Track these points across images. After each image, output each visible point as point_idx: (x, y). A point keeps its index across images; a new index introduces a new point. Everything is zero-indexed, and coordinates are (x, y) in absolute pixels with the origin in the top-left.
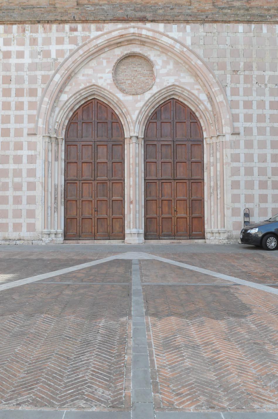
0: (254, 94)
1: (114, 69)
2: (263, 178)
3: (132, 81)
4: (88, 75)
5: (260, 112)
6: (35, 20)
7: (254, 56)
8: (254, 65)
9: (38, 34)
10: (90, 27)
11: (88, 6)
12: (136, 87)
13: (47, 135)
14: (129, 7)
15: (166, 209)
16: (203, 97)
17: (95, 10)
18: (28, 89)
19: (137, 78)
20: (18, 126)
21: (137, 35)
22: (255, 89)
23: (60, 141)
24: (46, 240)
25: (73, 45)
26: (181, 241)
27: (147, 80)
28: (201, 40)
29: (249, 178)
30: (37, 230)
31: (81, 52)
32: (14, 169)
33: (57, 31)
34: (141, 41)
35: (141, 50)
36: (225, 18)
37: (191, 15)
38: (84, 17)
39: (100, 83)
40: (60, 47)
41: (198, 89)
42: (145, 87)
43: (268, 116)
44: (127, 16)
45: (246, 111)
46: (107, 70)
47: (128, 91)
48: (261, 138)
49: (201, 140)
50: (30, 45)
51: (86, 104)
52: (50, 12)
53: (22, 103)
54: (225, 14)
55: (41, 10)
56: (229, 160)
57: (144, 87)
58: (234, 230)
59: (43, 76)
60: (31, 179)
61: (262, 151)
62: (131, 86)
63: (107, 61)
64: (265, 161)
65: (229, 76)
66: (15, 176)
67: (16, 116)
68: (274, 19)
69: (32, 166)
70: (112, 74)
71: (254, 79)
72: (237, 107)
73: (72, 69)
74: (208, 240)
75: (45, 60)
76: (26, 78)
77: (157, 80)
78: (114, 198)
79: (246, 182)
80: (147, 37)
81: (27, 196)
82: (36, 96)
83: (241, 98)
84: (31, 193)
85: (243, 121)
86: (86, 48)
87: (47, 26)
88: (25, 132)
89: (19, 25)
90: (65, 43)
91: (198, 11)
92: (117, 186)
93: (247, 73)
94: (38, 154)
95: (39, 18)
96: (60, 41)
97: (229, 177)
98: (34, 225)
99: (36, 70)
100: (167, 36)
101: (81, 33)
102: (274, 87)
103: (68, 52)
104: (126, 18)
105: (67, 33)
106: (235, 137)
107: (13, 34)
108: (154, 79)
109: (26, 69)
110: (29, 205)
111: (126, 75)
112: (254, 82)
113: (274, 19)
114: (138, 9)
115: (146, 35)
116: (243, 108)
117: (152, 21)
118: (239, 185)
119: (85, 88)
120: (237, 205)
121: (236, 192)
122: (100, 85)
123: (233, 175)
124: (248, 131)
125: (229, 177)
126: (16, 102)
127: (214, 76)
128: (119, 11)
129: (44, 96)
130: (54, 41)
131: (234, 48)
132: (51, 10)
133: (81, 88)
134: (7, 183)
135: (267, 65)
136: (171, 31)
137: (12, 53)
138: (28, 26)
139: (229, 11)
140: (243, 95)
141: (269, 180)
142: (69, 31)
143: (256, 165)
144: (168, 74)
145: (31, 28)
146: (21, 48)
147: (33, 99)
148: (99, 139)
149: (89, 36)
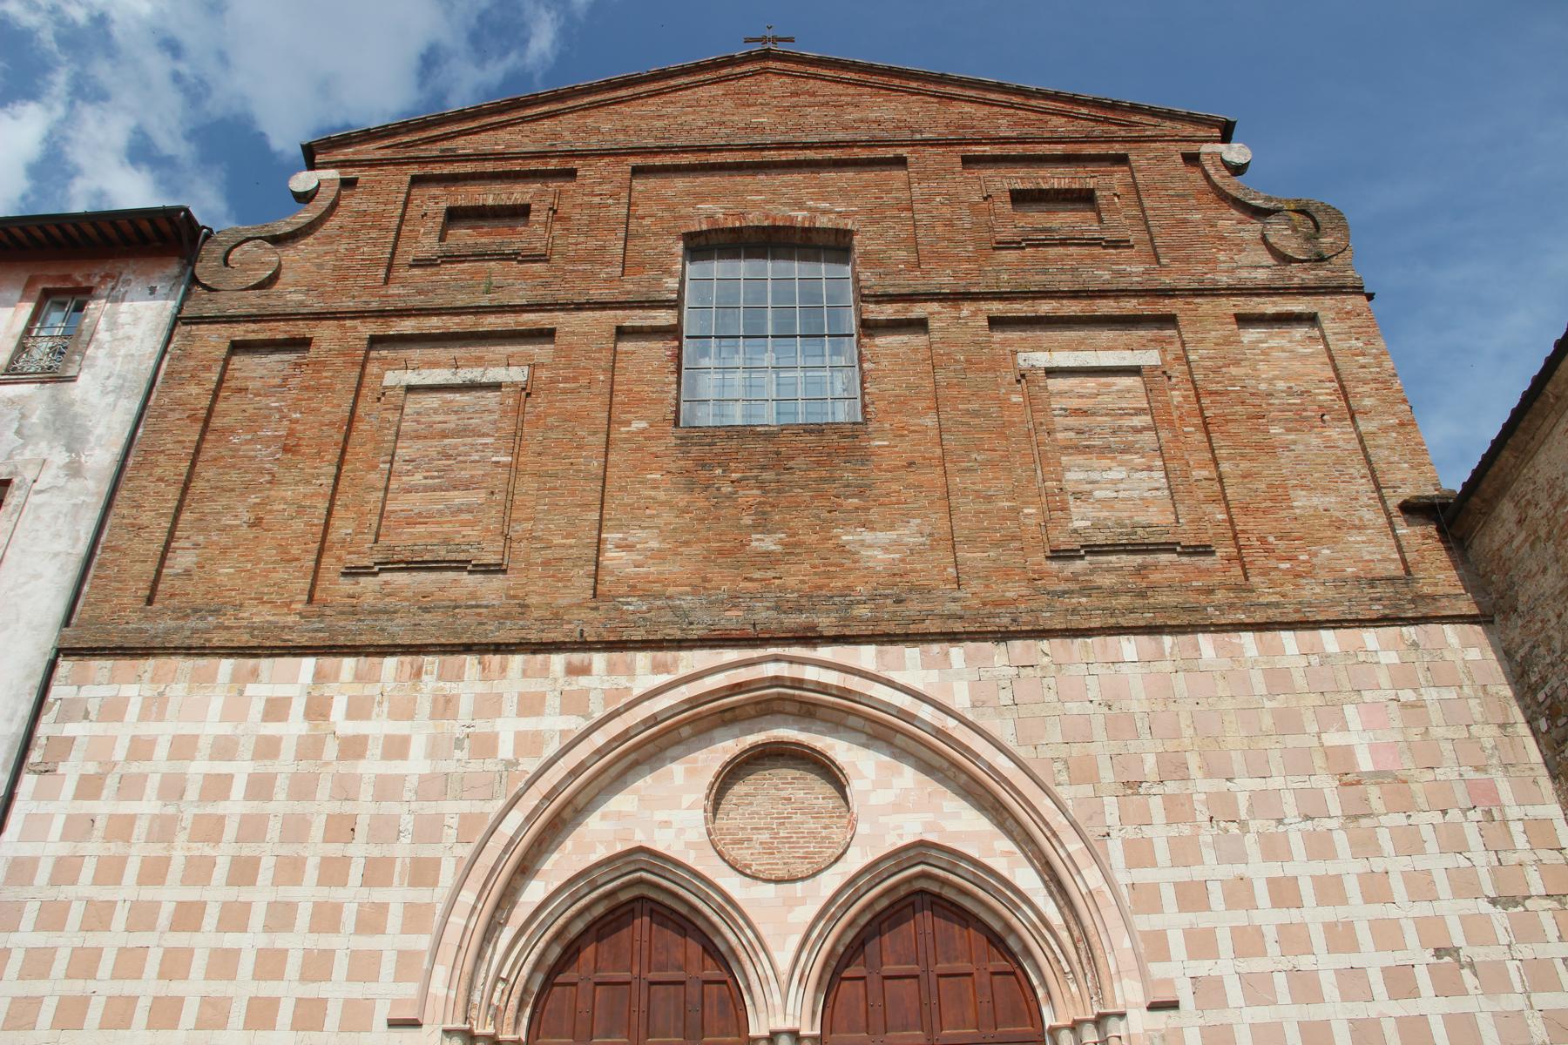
0: (1209, 856)
3: (775, 836)
4: (620, 815)
6: (457, 641)
8: (1193, 761)
9: (461, 684)
10: (633, 661)
11: (629, 599)
13: (459, 1025)
16: (1027, 879)
17: (649, 611)
18: (408, 861)
19: (790, 823)
20: (358, 990)
21: (788, 684)
22: (1210, 839)
27: (825, 828)
33: (525, 673)
36: (1076, 622)
38: (613, 630)
39: (662, 843)
40: (528, 724)
42: (821, 852)
43: (1271, 934)
45: (1188, 918)
46: (687, 799)
47: (761, 868)
55: (479, 614)
57: (815, 853)
59: (464, 818)
62: (769, 849)
65: (1111, 805)
68: (1232, 617)
70: (705, 811)
71: (1198, 806)
72: (1156, 907)
76: (407, 822)
77: (862, 828)
82: (435, 884)
83: (1164, 875)
86: (616, 727)
87: (494, 660)
89: (403, 658)
91: (984, 604)
93: (1171, 787)
95: (469, 634)
96: (530, 705)
99: (443, 795)
101: (603, 681)
102: (1274, 830)
104: (751, 630)
105: (556, 680)
107: (380, 685)
108: (852, 825)
109: (407, 795)
113: (1232, 617)
114: (790, 604)
115: (819, 683)
122: (660, 847)
126: (360, 905)
130: (510, 705)
131: (1115, 710)
132: (508, 613)
135: (1237, 757)
136: (901, 667)
137: (370, 742)
139: (1084, 600)
142: (563, 674)
144: (897, 807)
145: (442, 666)
146: (400, 728)
147: (421, 895)
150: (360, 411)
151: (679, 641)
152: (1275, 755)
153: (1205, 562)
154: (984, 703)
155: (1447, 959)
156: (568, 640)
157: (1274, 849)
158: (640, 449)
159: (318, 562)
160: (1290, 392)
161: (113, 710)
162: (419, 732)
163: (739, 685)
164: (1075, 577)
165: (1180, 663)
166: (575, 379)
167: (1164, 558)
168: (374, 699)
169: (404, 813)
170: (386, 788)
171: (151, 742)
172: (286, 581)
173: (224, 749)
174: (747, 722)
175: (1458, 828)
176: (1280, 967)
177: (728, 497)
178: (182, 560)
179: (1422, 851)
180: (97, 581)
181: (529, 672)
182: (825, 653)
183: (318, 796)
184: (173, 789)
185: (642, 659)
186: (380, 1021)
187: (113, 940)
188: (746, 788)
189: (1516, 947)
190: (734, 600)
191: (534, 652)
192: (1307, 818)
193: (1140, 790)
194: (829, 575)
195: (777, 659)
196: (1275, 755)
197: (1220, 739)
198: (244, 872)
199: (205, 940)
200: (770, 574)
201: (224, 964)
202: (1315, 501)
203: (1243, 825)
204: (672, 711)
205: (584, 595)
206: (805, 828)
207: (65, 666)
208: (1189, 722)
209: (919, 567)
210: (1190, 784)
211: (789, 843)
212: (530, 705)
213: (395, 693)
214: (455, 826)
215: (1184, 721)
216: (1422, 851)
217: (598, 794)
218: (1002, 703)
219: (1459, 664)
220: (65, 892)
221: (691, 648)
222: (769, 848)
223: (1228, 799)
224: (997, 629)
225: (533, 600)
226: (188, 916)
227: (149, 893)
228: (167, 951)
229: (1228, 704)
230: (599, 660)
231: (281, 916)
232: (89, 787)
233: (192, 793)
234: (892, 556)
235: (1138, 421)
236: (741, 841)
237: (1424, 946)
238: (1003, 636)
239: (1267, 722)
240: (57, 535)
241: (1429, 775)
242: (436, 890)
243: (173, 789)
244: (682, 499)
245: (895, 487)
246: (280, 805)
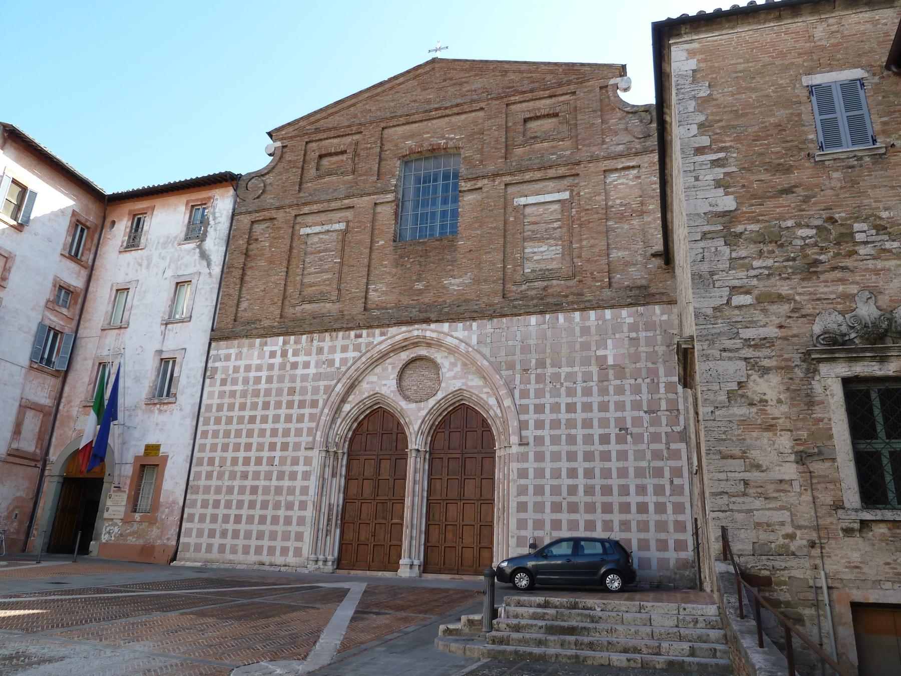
0: (548, 395)
2: (556, 499)
3: (418, 387)
4: (372, 383)
5: (554, 416)
8: (548, 361)
14: (415, 308)
15: (450, 536)
16: (492, 401)
20: (297, 439)
24: (312, 567)
29: (539, 499)
31: (364, 359)
34: (427, 343)
35: (427, 352)
36: (515, 311)
39: (384, 390)
40: (344, 355)
41: (487, 393)
43: (563, 422)
45: (536, 416)
48: (555, 448)
54: (515, 307)
56: (516, 477)
59: (325, 386)
60: (304, 498)
61: (556, 465)
62: (416, 392)
64: (559, 477)
65: (518, 377)
73: (355, 377)
75: (329, 370)
77: (443, 385)
78: (394, 521)
79: (535, 503)
80: (432, 339)
83: (531, 402)
86: (369, 355)
87: (334, 334)
88: (303, 445)
92: (397, 506)
93: (539, 371)
99: (319, 380)
100: (452, 336)
106: (522, 449)
108: (440, 384)
112: (547, 382)
117: (437, 321)
119: (369, 397)
120: (523, 533)
121: (522, 516)
122: (383, 392)
123: (519, 494)
124: (539, 440)
127: (501, 377)
129: (324, 407)
130: (339, 349)
133: (364, 396)
134: (280, 502)
135: (564, 360)
136: (456, 331)
138: (316, 336)
143: (548, 482)
144: (455, 378)
147: (314, 411)
148: (382, 453)
150: (294, 245)
155: (623, 432)
157: (571, 392)
159: (283, 303)
160: (621, 205)
161: (228, 358)
162: (313, 359)
165: (550, 325)
166: (360, 227)
169: (309, 385)
170: (304, 378)
171: (239, 367)
173: (259, 368)
175: (640, 385)
177: (409, 269)
178: (244, 305)
179: (624, 394)
180: (220, 315)
184: (246, 381)
187: (234, 427)
189: (649, 428)
192: (585, 382)
194: (439, 297)
198: (266, 406)
199: (257, 426)
200: (420, 298)
201: (262, 433)
202: (619, 254)
207: (213, 344)
212: (344, 349)
215: (548, 347)
216: (624, 394)
219: (658, 322)
220: (220, 414)
225: (345, 313)
226: (252, 419)
227: (242, 413)
228: (248, 430)
229: (564, 340)
231: (276, 419)
232: (224, 382)
233: (251, 382)
235: (555, 225)
237: (616, 427)
239: (578, 346)
240: (207, 299)
241: (634, 366)
243: (246, 381)
244: (394, 270)
245: (464, 261)
246: (275, 385)
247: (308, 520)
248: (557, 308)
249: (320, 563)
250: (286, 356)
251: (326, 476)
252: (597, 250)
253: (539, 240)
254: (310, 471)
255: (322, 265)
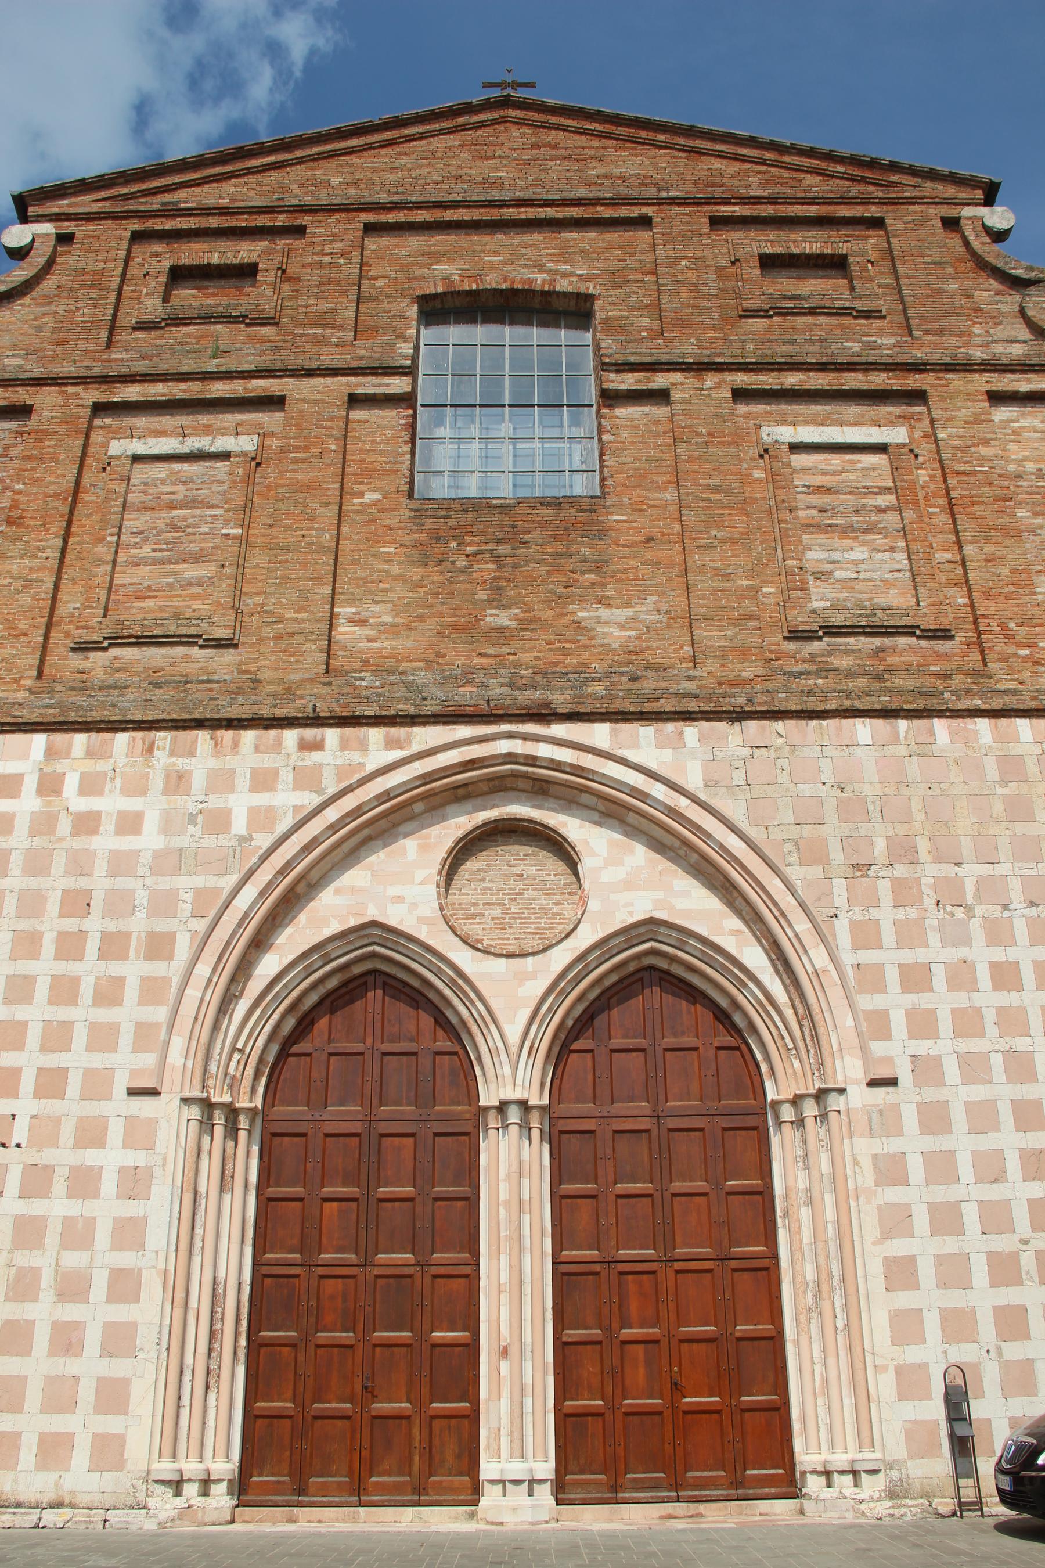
0: (934, 939)
1: (444, 873)
2: (1002, 1243)
3: (507, 911)
4: (353, 890)
6: (188, 717)
7: (919, 817)
8: (923, 845)
9: (193, 759)
11: (362, 675)
12: (521, 928)
17: (382, 686)
18: (143, 935)
20: (97, 1061)
21: (522, 761)
22: (935, 923)
23: (243, 1122)
25: (306, 793)
26: (702, 1508)
27: (556, 904)
28: (735, 772)
29: (950, 1245)
30: (129, 1466)
32: (65, 1218)
33: (257, 749)
37: (696, 697)
39: (395, 917)
40: (262, 799)
42: (552, 928)
44: (488, 701)
45: (911, 999)
46: (420, 875)
49: (759, 1111)
50: (166, 792)
51: (344, 990)
52: (239, 694)
53: (119, 981)
55: (211, 690)
58: (911, 1458)
59: (198, 893)
60: (127, 1259)
61: (988, 1142)
62: (501, 924)
63: (419, 845)
64: (999, 1177)
65: (839, 886)
66: (66, 1245)
67: (94, 1028)
68: (968, 702)
69: (133, 1209)
74: (813, 1503)
76: (142, 897)
77: (593, 905)
81: (106, 1325)
82: (170, 957)
84: (121, 1313)
85: (905, 1035)
86: (349, 803)
87: (227, 735)
89: (134, 734)
90: (280, 787)
91: (720, 684)
93: (900, 871)
94: (160, 1162)
97: (874, 1244)
98: (120, 1440)
99: (177, 870)
101: (335, 757)
102: (998, 915)
103: (290, 814)
104: (485, 707)
107: (112, 761)
108: (584, 902)
109: (141, 871)
110: (108, 1359)
111: (485, 889)
113: (968, 702)
114: (524, 681)
116: (899, 989)
118: (915, 1274)
120: (913, 1354)
121: (904, 1300)
122: (393, 922)
125: (874, 1244)
128: (460, 689)
130: (243, 780)
131: (848, 793)
132: (240, 688)
134: (35, 1273)
135: (966, 843)
136: (636, 746)
137: (103, 817)
139: (820, 681)
140: (895, 945)
141: (1024, 1247)
142: (296, 749)
144: (628, 885)
146: (134, 804)
147: (157, 968)
149: (361, 765)
150: (85, 481)
151: (413, 717)
152: (1004, 843)
153: (943, 646)
154: (717, 782)
156: (300, 715)
158: (373, 521)
159: (46, 637)
163: (472, 761)
164: (812, 659)
165: (914, 747)
166: (306, 449)
167: (903, 641)
168: (106, 775)
172: (14, 656)
174: (480, 799)
176: (997, 1047)
177: (463, 571)
181: (262, 748)
182: (558, 730)
183: (53, 871)
185: (375, 735)
186: (120, 1089)
188: (478, 864)
190: (468, 675)
191: (267, 727)
192: (1033, 904)
193: (869, 872)
195: (510, 736)
196: (1004, 843)
197: (951, 824)
200: (505, 650)
203: (969, 910)
204: (405, 787)
205: (316, 670)
206: (536, 904)
208: (920, 807)
209: (655, 645)
210: (919, 868)
211: (521, 918)
212: (263, 781)
213: (127, 769)
214: (190, 900)
215: (916, 806)
217: (331, 869)
218: (735, 783)
221: (424, 724)
222: (501, 924)
223: (955, 884)
224: (732, 709)
225: (265, 675)
229: (960, 790)
230: (332, 735)
234: (628, 633)
235: (882, 501)
236: (473, 917)
238: (738, 716)
239: (998, 808)
242: (173, 963)
244: (416, 573)
245: (632, 563)
247: (147, 1337)
248: (546, 502)
249: (191, 1490)
250: (57, 792)
251: (202, 1188)
252: (1006, 571)
253: (847, 530)
254: (150, 1168)
255: (175, 542)
